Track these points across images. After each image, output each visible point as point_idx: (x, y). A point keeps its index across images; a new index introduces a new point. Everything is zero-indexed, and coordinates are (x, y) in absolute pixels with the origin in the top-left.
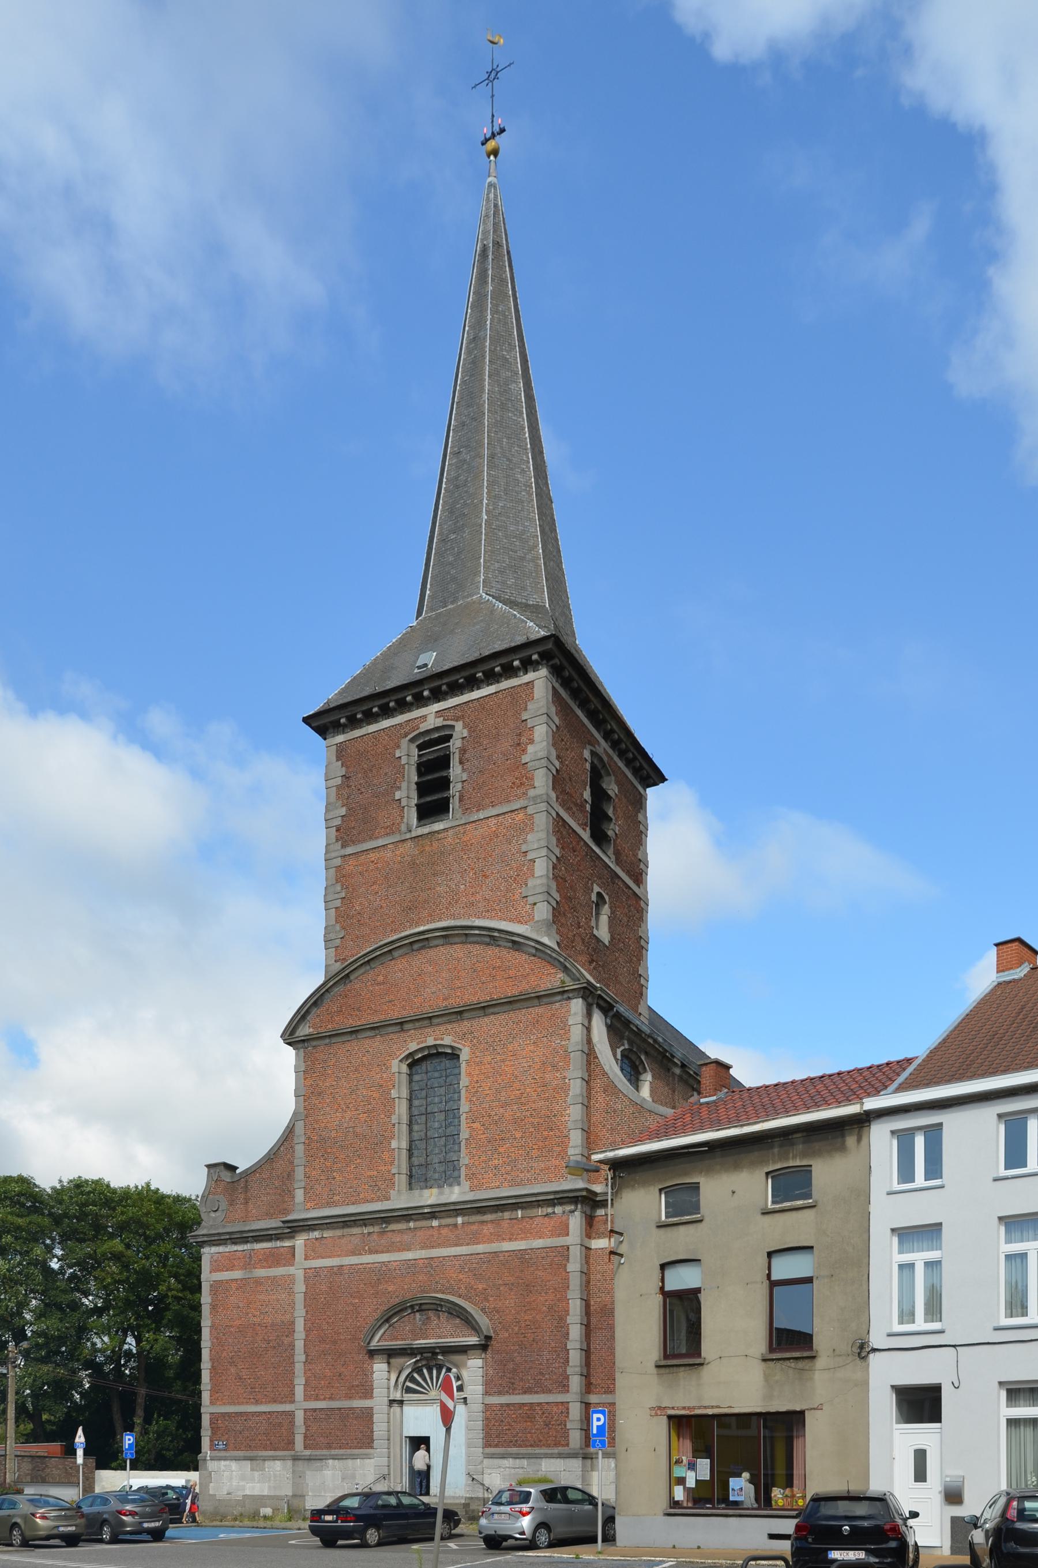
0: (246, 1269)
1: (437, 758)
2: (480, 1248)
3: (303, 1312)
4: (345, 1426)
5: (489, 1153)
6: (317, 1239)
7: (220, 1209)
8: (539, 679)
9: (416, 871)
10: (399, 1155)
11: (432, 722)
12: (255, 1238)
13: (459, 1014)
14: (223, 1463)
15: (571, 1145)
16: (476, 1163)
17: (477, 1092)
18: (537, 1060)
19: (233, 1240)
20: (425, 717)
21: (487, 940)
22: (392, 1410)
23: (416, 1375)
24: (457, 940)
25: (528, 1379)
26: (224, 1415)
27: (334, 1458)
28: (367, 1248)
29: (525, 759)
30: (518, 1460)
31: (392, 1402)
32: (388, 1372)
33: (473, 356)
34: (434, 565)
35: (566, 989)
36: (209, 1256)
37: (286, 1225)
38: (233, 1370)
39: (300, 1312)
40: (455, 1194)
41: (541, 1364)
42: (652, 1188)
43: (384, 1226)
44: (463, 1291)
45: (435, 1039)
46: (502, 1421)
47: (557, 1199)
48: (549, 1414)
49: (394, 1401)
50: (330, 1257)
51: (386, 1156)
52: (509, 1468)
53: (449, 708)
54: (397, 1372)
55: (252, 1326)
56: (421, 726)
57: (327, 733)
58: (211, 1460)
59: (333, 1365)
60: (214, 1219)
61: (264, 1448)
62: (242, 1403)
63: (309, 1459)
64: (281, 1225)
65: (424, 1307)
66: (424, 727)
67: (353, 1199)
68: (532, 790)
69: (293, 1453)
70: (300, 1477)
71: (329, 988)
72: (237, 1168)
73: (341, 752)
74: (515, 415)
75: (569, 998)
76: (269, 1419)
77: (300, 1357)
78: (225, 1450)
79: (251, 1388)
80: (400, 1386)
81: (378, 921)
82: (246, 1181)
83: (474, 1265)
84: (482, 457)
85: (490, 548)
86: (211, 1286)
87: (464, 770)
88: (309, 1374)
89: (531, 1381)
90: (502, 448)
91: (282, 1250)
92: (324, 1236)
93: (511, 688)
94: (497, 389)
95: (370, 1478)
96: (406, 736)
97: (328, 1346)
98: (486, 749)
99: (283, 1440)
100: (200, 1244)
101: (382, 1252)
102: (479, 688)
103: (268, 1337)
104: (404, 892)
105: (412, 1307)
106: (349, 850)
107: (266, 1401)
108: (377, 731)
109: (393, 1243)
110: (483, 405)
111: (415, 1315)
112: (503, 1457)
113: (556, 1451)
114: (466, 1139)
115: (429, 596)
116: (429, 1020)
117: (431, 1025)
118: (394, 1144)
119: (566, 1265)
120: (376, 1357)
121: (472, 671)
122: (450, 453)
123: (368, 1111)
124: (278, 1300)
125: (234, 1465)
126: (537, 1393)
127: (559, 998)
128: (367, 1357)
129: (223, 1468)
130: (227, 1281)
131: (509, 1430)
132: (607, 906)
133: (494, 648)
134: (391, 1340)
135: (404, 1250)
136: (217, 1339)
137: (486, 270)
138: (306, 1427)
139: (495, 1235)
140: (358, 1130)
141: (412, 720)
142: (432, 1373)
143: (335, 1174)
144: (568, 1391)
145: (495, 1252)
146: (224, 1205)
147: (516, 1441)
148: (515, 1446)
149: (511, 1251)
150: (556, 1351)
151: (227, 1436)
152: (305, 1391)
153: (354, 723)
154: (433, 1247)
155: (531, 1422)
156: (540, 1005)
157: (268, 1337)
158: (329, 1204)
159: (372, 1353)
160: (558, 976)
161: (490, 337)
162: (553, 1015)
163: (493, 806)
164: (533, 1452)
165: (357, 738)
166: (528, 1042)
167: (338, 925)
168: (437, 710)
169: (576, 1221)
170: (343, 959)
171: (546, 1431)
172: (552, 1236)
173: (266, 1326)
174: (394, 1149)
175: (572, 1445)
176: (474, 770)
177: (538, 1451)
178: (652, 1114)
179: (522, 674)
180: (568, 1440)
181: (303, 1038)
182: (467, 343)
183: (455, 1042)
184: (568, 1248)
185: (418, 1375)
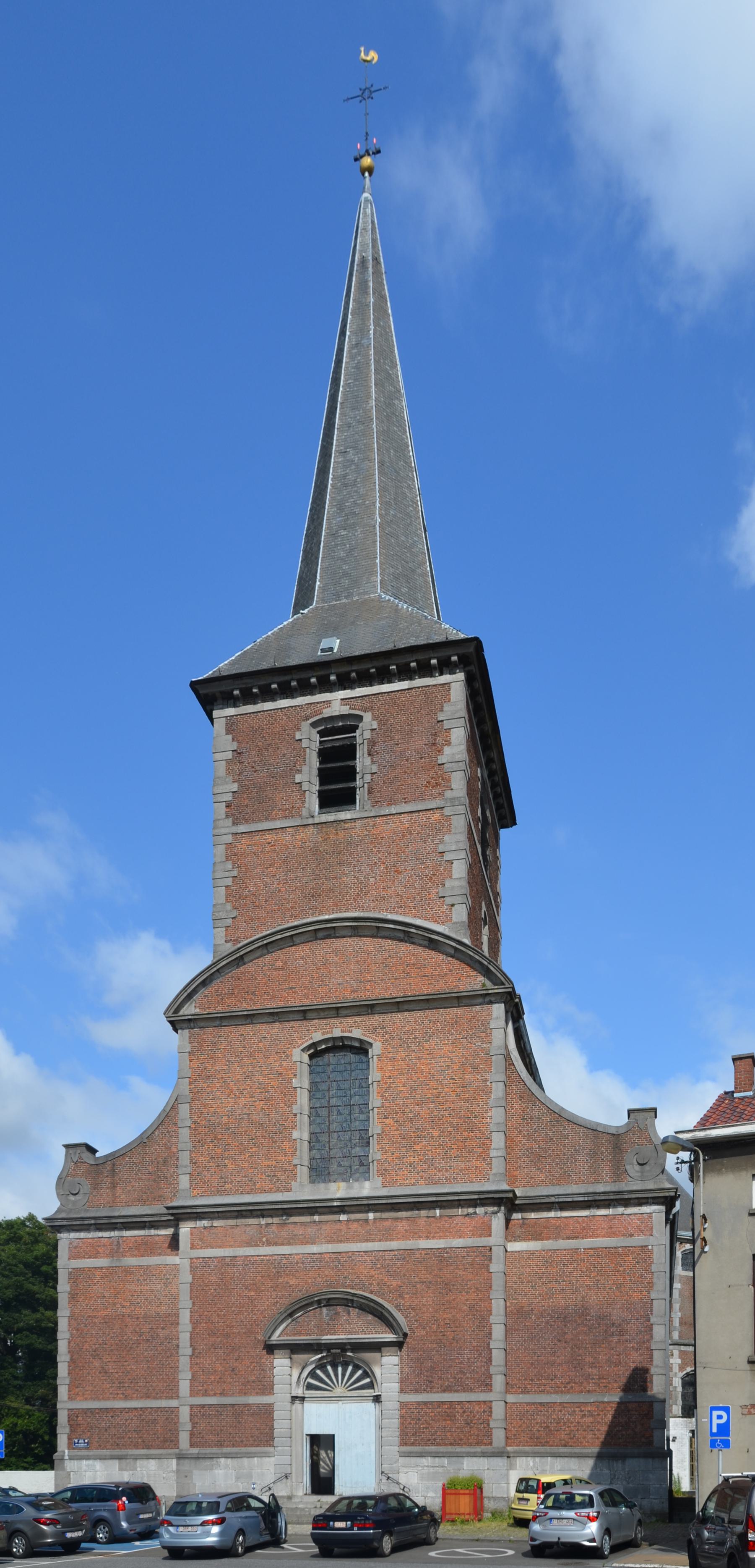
0: (112, 1257)
1: (343, 746)
2: (394, 1245)
3: (189, 1304)
4: (239, 1422)
5: (404, 1150)
6: (205, 1228)
7: (80, 1193)
8: (456, 682)
9: (319, 858)
10: (301, 1146)
12: (125, 1225)
13: (369, 1008)
14: (84, 1462)
15: (493, 1146)
16: (389, 1159)
17: (389, 1087)
18: (455, 1060)
19: (98, 1226)
20: (328, 703)
21: (401, 935)
22: (294, 1407)
23: (318, 1372)
24: (367, 932)
25: (447, 1378)
26: (85, 1411)
27: (227, 1456)
28: (264, 1239)
29: (442, 759)
30: (437, 1459)
31: (294, 1398)
32: (291, 1367)
33: (356, 362)
34: (322, 558)
35: (490, 992)
36: (67, 1242)
37: (171, 1211)
38: (97, 1363)
39: (185, 1303)
40: (366, 1189)
41: (461, 1363)
42: (744, 1173)
43: (284, 1218)
44: (375, 1287)
45: (342, 1031)
46: (419, 1419)
47: (480, 1199)
48: (470, 1412)
49: (297, 1397)
50: (220, 1247)
51: (286, 1145)
52: (428, 1466)
53: (356, 697)
54: (300, 1368)
55: (121, 1317)
56: (325, 711)
57: (215, 703)
58: (70, 1459)
59: (224, 1360)
60: (74, 1203)
61: (134, 1445)
62: (108, 1399)
63: (197, 1458)
64: (165, 1211)
65: (332, 1302)
66: (327, 713)
67: (248, 1188)
68: (450, 791)
69: (177, 1451)
70: (186, 1477)
71: (221, 968)
73: (231, 726)
74: (399, 431)
75: (491, 1003)
76: (141, 1415)
77: (186, 1350)
78: (86, 1448)
79: (120, 1383)
80: (302, 1383)
81: (275, 904)
82: (114, 1165)
83: (387, 1262)
84: (371, 460)
85: (384, 551)
86: (70, 1274)
87: (373, 762)
88: (196, 1368)
89: (452, 1380)
90: (389, 457)
91: (157, 1238)
92: (215, 1225)
93: (426, 687)
94: (382, 399)
95: (270, 1478)
96: (307, 720)
97: (219, 1340)
98: (397, 744)
99: (158, 1438)
100: (57, 1228)
101: (283, 1244)
102: (390, 682)
103: (140, 1329)
104: (305, 879)
105: (319, 1302)
106: (242, 828)
107: (137, 1397)
108: (274, 710)
109: (295, 1235)
110: (370, 411)
111: (321, 1310)
112: (421, 1455)
113: (478, 1449)
114: (378, 1134)
115: (319, 587)
116: (336, 1011)
117: (338, 1017)
118: (295, 1135)
119: (488, 1266)
120: (276, 1351)
121: (386, 662)
122: (335, 451)
123: (266, 1100)
124: (152, 1291)
126: (457, 1391)
127: (480, 1000)
128: (265, 1352)
129: (84, 1468)
130: (90, 1269)
131: (426, 1428)
132: (487, 927)
133: (409, 643)
134: (294, 1335)
135: (307, 1243)
136: (78, 1330)
137: (366, 281)
138: (193, 1423)
139: (410, 1233)
140: (254, 1117)
141: (314, 703)
142: (337, 1370)
143: (226, 1161)
144: (491, 1390)
145: (410, 1250)
146: (86, 1187)
147: (435, 1439)
148: (433, 1444)
149: (428, 1249)
150: (477, 1351)
151: (89, 1433)
152: (191, 1386)
153: (248, 698)
154: (341, 1241)
155: (451, 1420)
156: (459, 1007)
157: (140, 1329)
158: (220, 1192)
159: (271, 1349)
160: (479, 979)
161: (374, 347)
162: (474, 1017)
163: (405, 802)
164: (453, 1450)
165: (250, 713)
166: (446, 1042)
167: (230, 904)
168: (342, 697)
169: (498, 1222)
170: (234, 940)
171: (467, 1429)
172: (473, 1235)
173: (138, 1318)
174: (295, 1140)
175: (495, 1444)
176: (384, 763)
177: (458, 1449)
178: (570, 1123)
179: (437, 675)
180: (491, 1439)
181: (190, 1017)
182: (348, 348)
183: (364, 1035)
184: (491, 1249)
185: (321, 1371)
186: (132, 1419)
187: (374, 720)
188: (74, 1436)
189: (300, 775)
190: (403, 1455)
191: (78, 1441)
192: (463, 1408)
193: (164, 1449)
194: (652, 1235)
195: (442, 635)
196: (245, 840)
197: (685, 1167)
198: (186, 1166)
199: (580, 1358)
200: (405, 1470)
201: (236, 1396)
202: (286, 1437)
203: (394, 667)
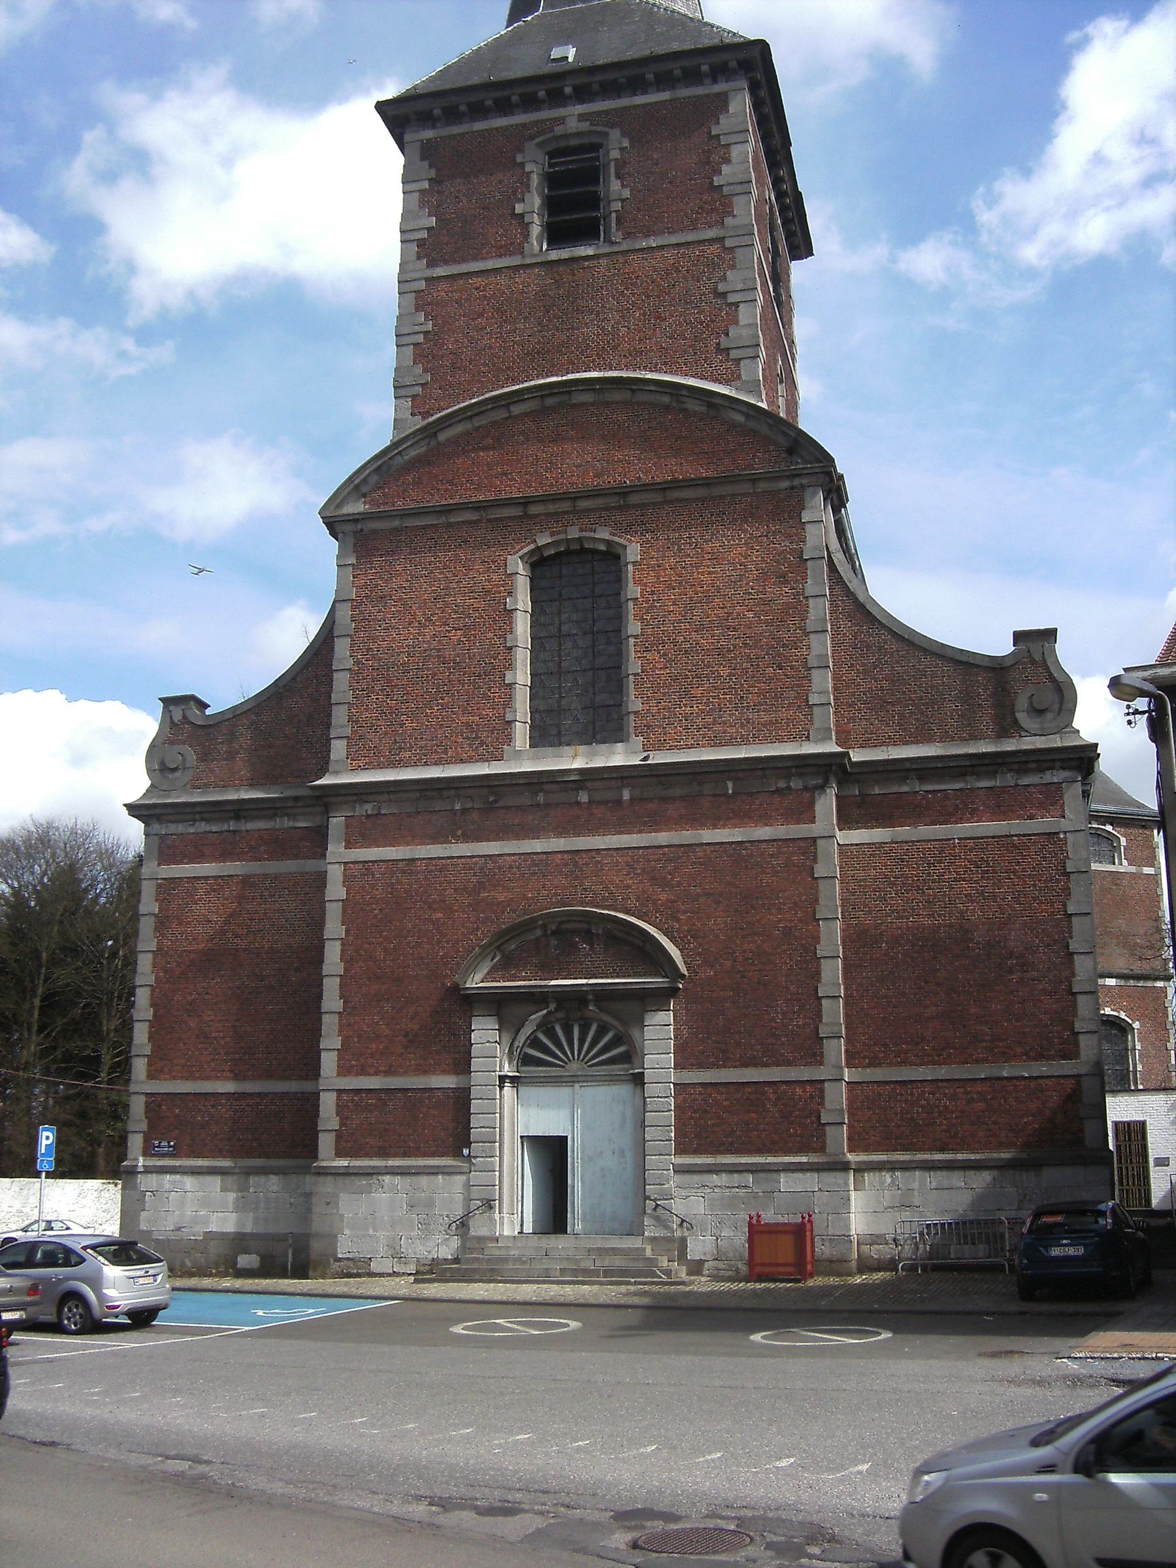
6: (368, 816)
11: (573, 125)
20: (562, 120)
29: (717, 181)
45: (581, 530)
46: (706, 1111)
62: (207, 1078)
63: (347, 1173)
66: (559, 130)
70: (328, 1204)
72: (207, 706)
76: (258, 1104)
81: (485, 365)
86: (159, 886)
87: (623, 186)
92: (383, 812)
106: (440, 271)
114: (635, 675)
125: (189, 1182)
126: (766, 1065)
129: (167, 1186)
136: (166, 972)
144: (821, 1063)
186: (243, 1111)
187: (625, 137)
188: (154, 1136)
189: (522, 205)
190: (680, 1170)
191: (160, 1143)
192: (777, 1093)
193: (293, 1158)
194: (1064, 817)
195: (715, 38)
196: (443, 286)
197: (1142, 721)
198: (342, 727)
199: (960, 1008)
200: (684, 1193)
201: (410, 1075)
202: (489, 1142)
203: (652, 76)
